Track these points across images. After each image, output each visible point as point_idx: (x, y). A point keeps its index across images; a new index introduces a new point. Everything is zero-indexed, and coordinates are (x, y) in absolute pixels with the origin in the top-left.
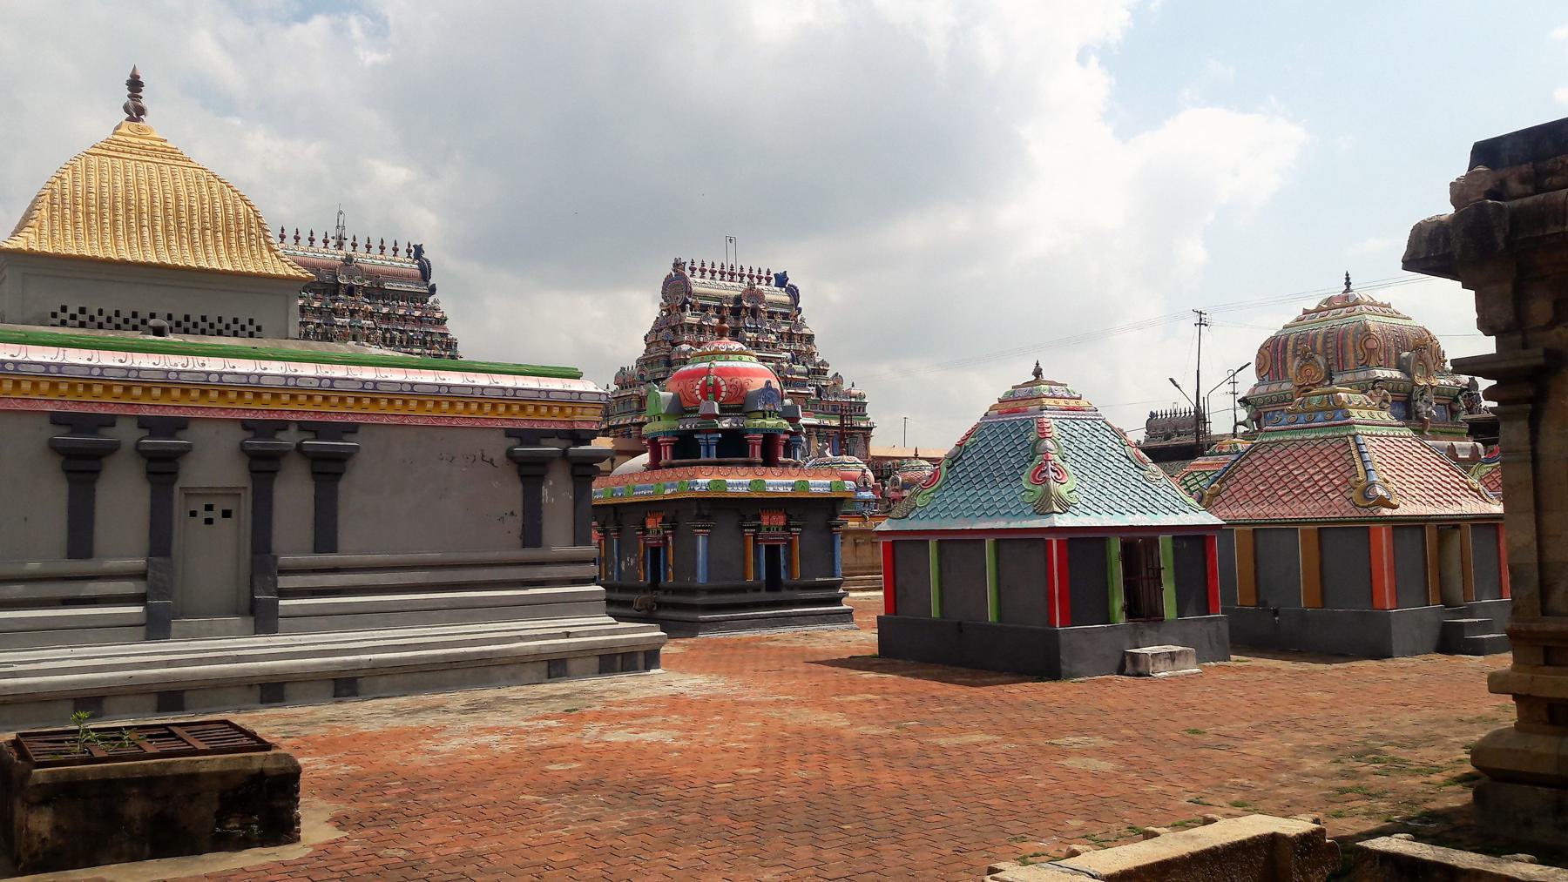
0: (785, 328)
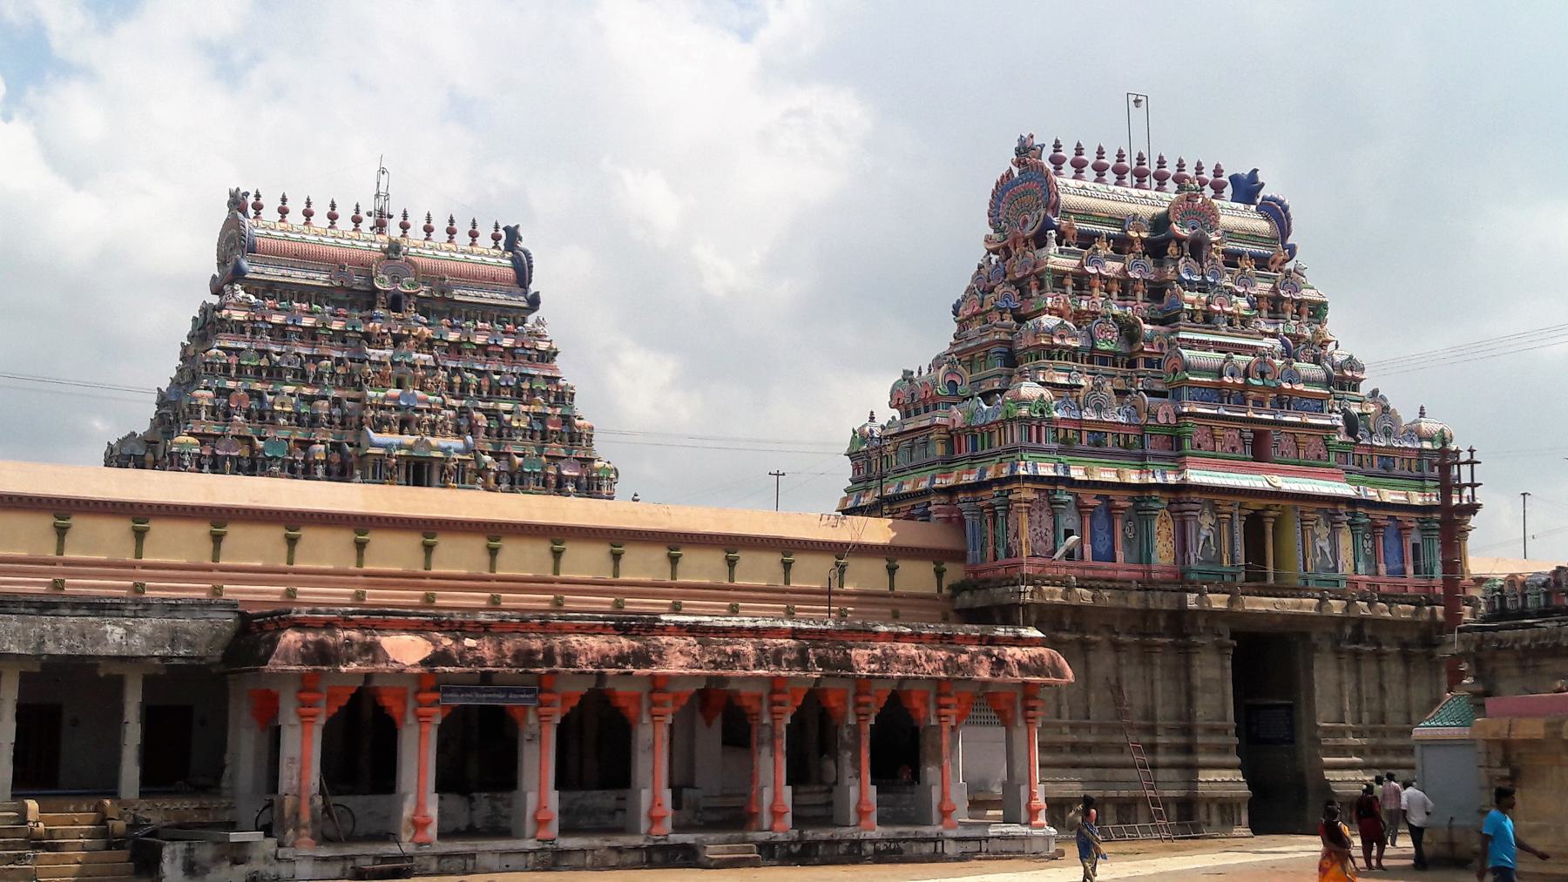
0: (1263, 287)
